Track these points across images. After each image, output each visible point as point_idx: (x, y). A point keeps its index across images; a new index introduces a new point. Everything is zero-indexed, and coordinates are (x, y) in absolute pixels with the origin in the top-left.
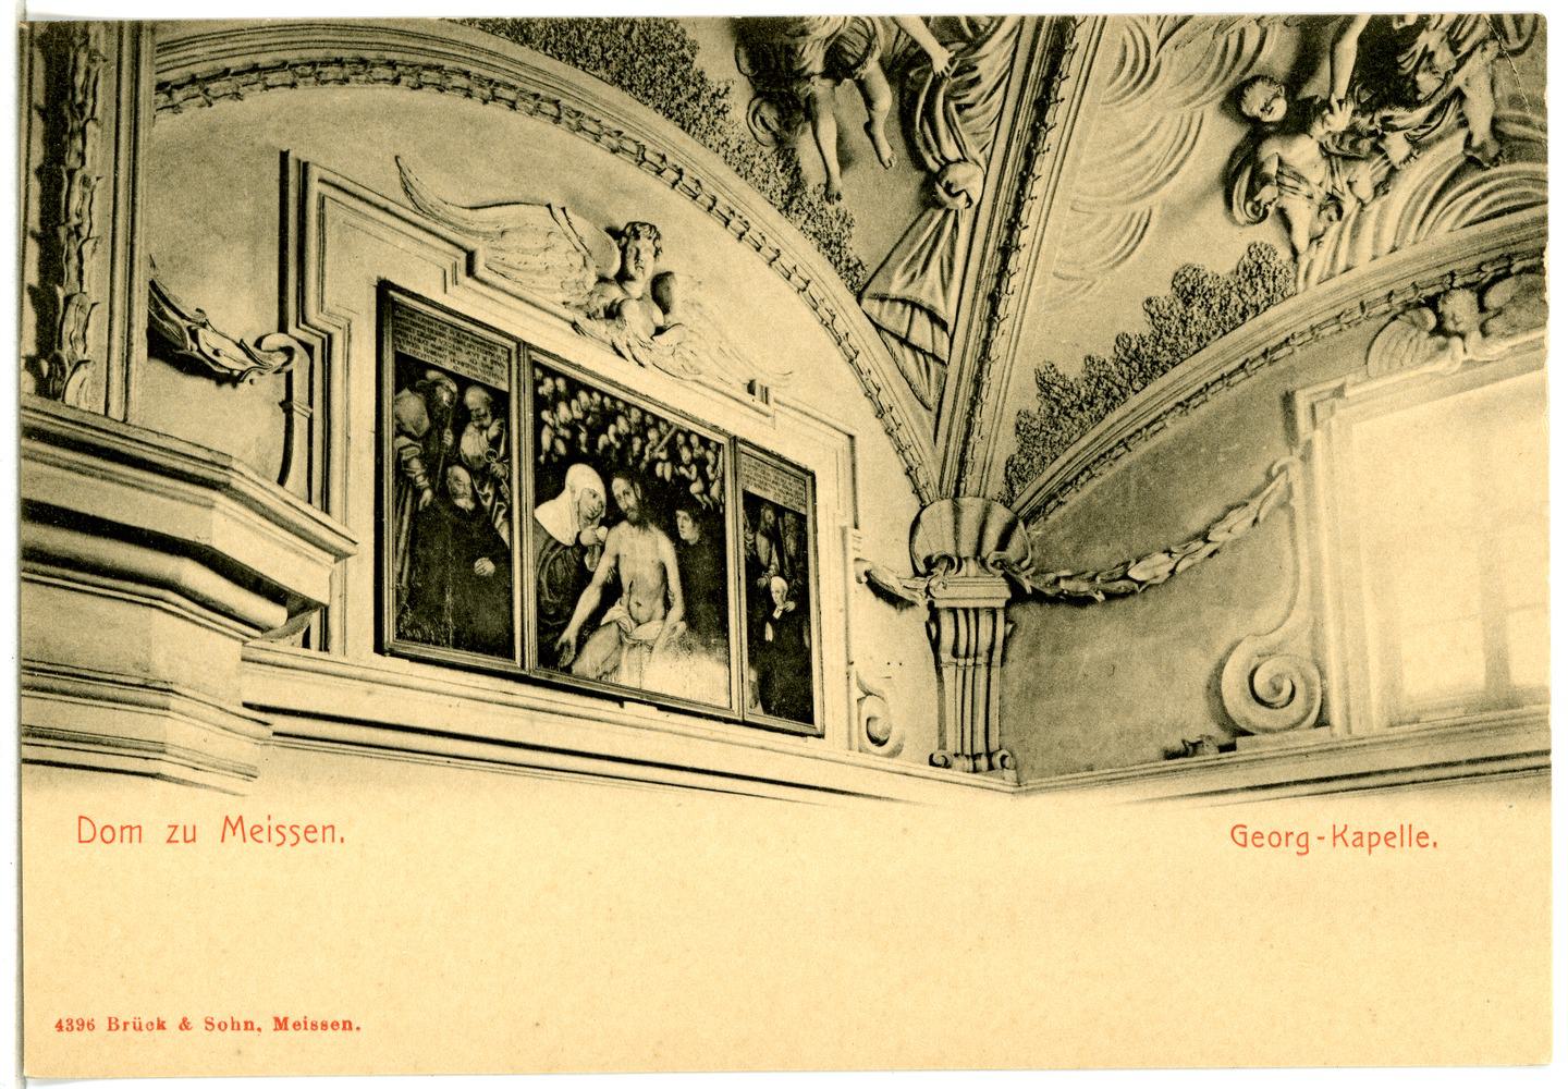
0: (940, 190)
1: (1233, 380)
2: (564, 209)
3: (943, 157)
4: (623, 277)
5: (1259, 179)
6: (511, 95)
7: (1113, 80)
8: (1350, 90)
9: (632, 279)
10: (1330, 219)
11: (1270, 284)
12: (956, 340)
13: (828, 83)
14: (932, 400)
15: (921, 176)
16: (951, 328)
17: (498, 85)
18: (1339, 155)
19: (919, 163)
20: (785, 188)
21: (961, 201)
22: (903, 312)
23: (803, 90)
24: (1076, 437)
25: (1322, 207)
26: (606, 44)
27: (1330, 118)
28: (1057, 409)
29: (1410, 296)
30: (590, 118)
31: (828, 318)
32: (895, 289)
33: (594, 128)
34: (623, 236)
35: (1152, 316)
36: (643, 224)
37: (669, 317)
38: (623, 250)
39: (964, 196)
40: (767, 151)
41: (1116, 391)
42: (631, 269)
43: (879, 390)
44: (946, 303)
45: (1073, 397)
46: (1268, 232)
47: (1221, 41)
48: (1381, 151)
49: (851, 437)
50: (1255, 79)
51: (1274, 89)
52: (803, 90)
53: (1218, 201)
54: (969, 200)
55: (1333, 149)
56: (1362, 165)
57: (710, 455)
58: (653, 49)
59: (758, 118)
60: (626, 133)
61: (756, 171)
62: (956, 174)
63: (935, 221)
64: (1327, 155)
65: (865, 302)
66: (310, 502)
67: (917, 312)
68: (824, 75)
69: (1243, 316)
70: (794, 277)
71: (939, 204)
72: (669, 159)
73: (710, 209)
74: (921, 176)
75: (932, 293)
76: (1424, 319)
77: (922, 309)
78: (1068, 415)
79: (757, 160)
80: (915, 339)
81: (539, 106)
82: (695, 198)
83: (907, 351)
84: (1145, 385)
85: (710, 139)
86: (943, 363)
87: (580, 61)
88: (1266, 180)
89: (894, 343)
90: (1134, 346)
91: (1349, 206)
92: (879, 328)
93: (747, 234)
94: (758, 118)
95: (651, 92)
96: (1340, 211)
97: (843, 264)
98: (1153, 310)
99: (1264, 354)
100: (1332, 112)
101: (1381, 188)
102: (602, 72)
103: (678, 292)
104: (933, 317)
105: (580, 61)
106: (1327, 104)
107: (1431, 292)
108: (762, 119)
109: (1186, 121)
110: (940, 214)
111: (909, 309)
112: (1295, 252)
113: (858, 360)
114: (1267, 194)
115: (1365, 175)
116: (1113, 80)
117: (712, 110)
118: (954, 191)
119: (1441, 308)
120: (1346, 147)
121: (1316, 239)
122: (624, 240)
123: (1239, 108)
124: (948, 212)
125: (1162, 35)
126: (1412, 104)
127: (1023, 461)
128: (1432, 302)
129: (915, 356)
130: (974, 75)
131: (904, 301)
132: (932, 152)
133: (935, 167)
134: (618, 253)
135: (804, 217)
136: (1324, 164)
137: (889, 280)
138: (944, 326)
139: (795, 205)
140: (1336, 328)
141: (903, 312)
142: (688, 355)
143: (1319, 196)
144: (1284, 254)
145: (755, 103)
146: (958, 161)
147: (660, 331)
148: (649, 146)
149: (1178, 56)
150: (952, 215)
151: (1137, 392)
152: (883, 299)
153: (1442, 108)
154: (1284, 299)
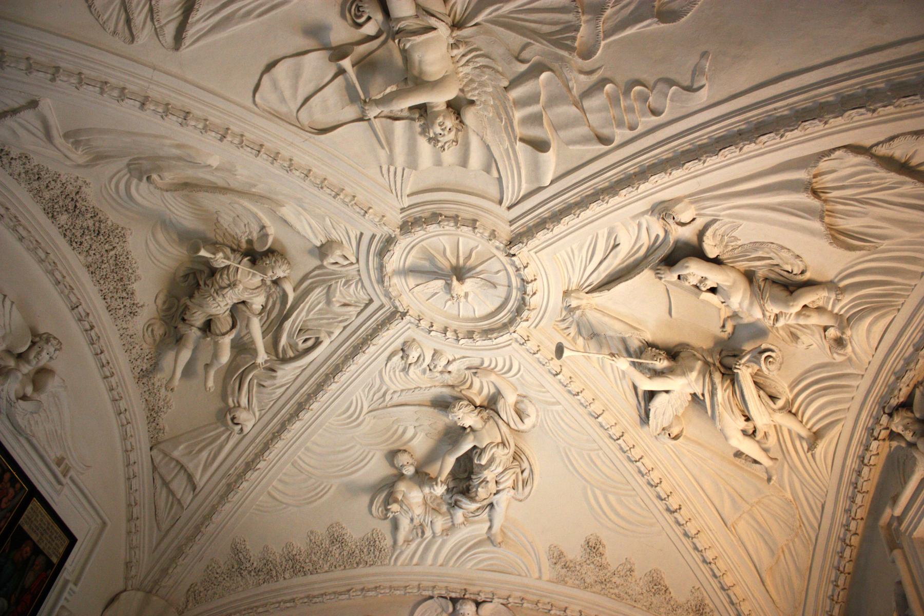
0: (229, 417)
1: (340, 597)
2: (13, 303)
3: (238, 402)
4: (21, 357)
5: (390, 498)
6: (24, 233)
7: (339, 415)
8: (447, 479)
9: (28, 362)
10: (417, 534)
11: (377, 553)
12: (197, 498)
13: (199, 333)
14: (164, 527)
15: (222, 405)
16: (197, 490)
17: (20, 225)
18: (431, 507)
19: (224, 397)
20: (144, 369)
21: (238, 428)
22: (174, 468)
23: (182, 327)
24: (240, 589)
25: (415, 528)
26: (94, 247)
27: (435, 487)
28: (236, 567)
29: (443, 592)
30: (60, 272)
31: (129, 448)
32: (176, 454)
33: (59, 277)
34: (38, 339)
35: (311, 540)
36: (55, 338)
37: (35, 396)
38: (33, 343)
39: (239, 427)
40: (145, 346)
41: (274, 573)
42: (32, 355)
43: (136, 504)
44: (202, 475)
45: (248, 565)
46: (385, 527)
47: (396, 427)
48: (451, 514)
49: (104, 523)
50: (405, 451)
51: (411, 461)
52: (182, 327)
53: (366, 499)
54: (242, 430)
55: (429, 502)
56: (440, 518)
57: (11, 491)
58: (117, 264)
59: (150, 329)
60: (76, 291)
61: (134, 351)
62: (242, 416)
63: (218, 431)
64: (425, 503)
65: (155, 451)
66: (294, 290)
67: (182, 472)
68: (200, 329)
69: (358, 564)
70: (122, 415)
71: (225, 424)
72: (91, 318)
73: (97, 354)
74: (222, 405)
75: (197, 467)
76: (448, 607)
77: (186, 470)
78: (241, 574)
79: (137, 347)
80: (174, 486)
81: (36, 248)
82: (93, 344)
83: (164, 491)
84: (292, 577)
85: (119, 322)
86: (183, 507)
87: (74, 244)
88: (396, 501)
89: (159, 482)
90: (294, 553)
91: (428, 533)
92: (155, 468)
93: (110, 379)
94: (150, 329)
95: (102, 282)
96: (423, 533)
97: (154, 424)
98: (312, 538)
99: (363, 589)
100: (437, 484)
101: (447, 531)
102: (81, 258)
103: (53, 385)
104: (190, 478)
105: (74, 244)
106: (436, 479)
107: (453, 595)
108: (152, 331)
109: (365, 454)
110: (223, 429)
111: (178, 467)
112: (395, 542)
113: (134, 481)
114: (395, 507)
115: (440, 523)
116: (339, 415)
117: (129, 310)
118: (236, 421)
119: (458, 607)
120: (435, 504)
121: (408, 542)
122: (37, 339)
123: (393, 461)
124: (227, 429)
125: (370, 408)
126: (473, 499)
127: (202, 589)
128: (454, 601)
129: (168, 497)
130: (274, 374)
131: (178, 462)
132: (233, 397)
133: (231, 404)
134: (29, 344)
135: (146, 389)
136: (423, 507)
137: (176, 447)
138: (194, 488)
139: (145, 380)
140: (402, 592)
141: (174, 468)
142: (32, 422)
143: (416, 522)
144: (389, 542)
145: (153, 321)
146: (245, 408)
147: (24, 398)
148: (84, 305)
149: (373, 421)
150: (229, 433)
151: (285, 579)
152: (166, 455)
153: (482, 508)
154: (382, 565)
